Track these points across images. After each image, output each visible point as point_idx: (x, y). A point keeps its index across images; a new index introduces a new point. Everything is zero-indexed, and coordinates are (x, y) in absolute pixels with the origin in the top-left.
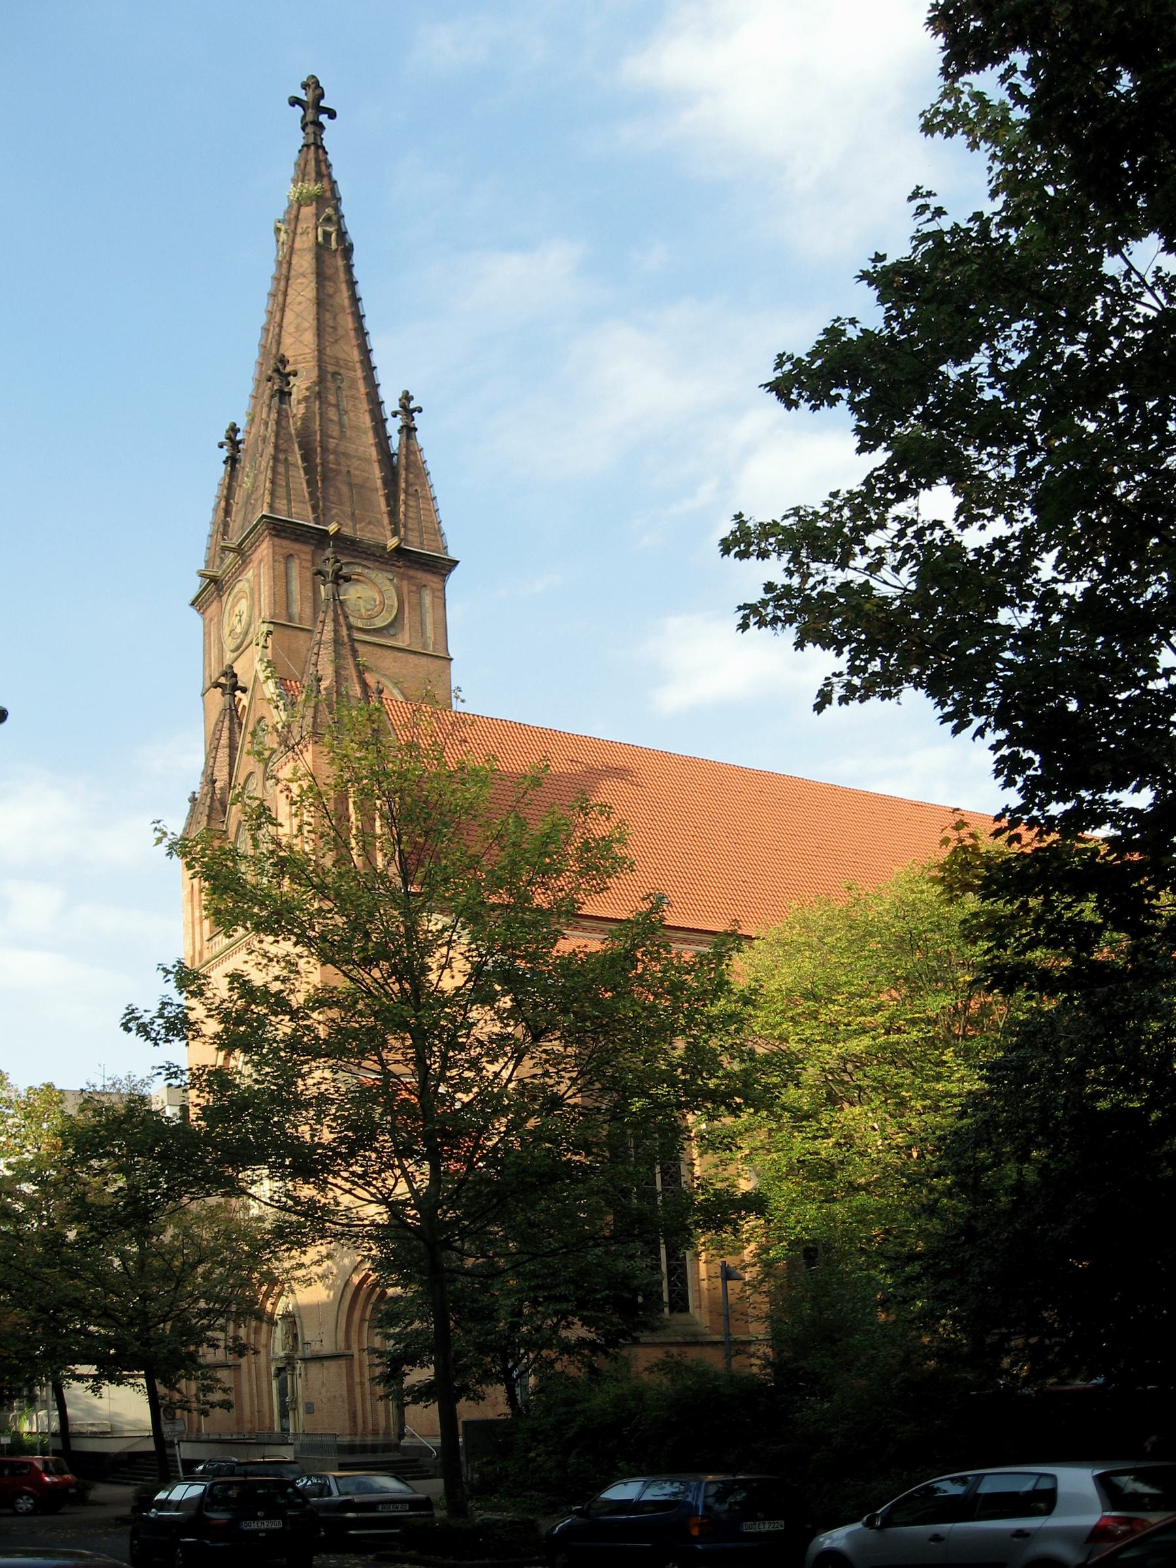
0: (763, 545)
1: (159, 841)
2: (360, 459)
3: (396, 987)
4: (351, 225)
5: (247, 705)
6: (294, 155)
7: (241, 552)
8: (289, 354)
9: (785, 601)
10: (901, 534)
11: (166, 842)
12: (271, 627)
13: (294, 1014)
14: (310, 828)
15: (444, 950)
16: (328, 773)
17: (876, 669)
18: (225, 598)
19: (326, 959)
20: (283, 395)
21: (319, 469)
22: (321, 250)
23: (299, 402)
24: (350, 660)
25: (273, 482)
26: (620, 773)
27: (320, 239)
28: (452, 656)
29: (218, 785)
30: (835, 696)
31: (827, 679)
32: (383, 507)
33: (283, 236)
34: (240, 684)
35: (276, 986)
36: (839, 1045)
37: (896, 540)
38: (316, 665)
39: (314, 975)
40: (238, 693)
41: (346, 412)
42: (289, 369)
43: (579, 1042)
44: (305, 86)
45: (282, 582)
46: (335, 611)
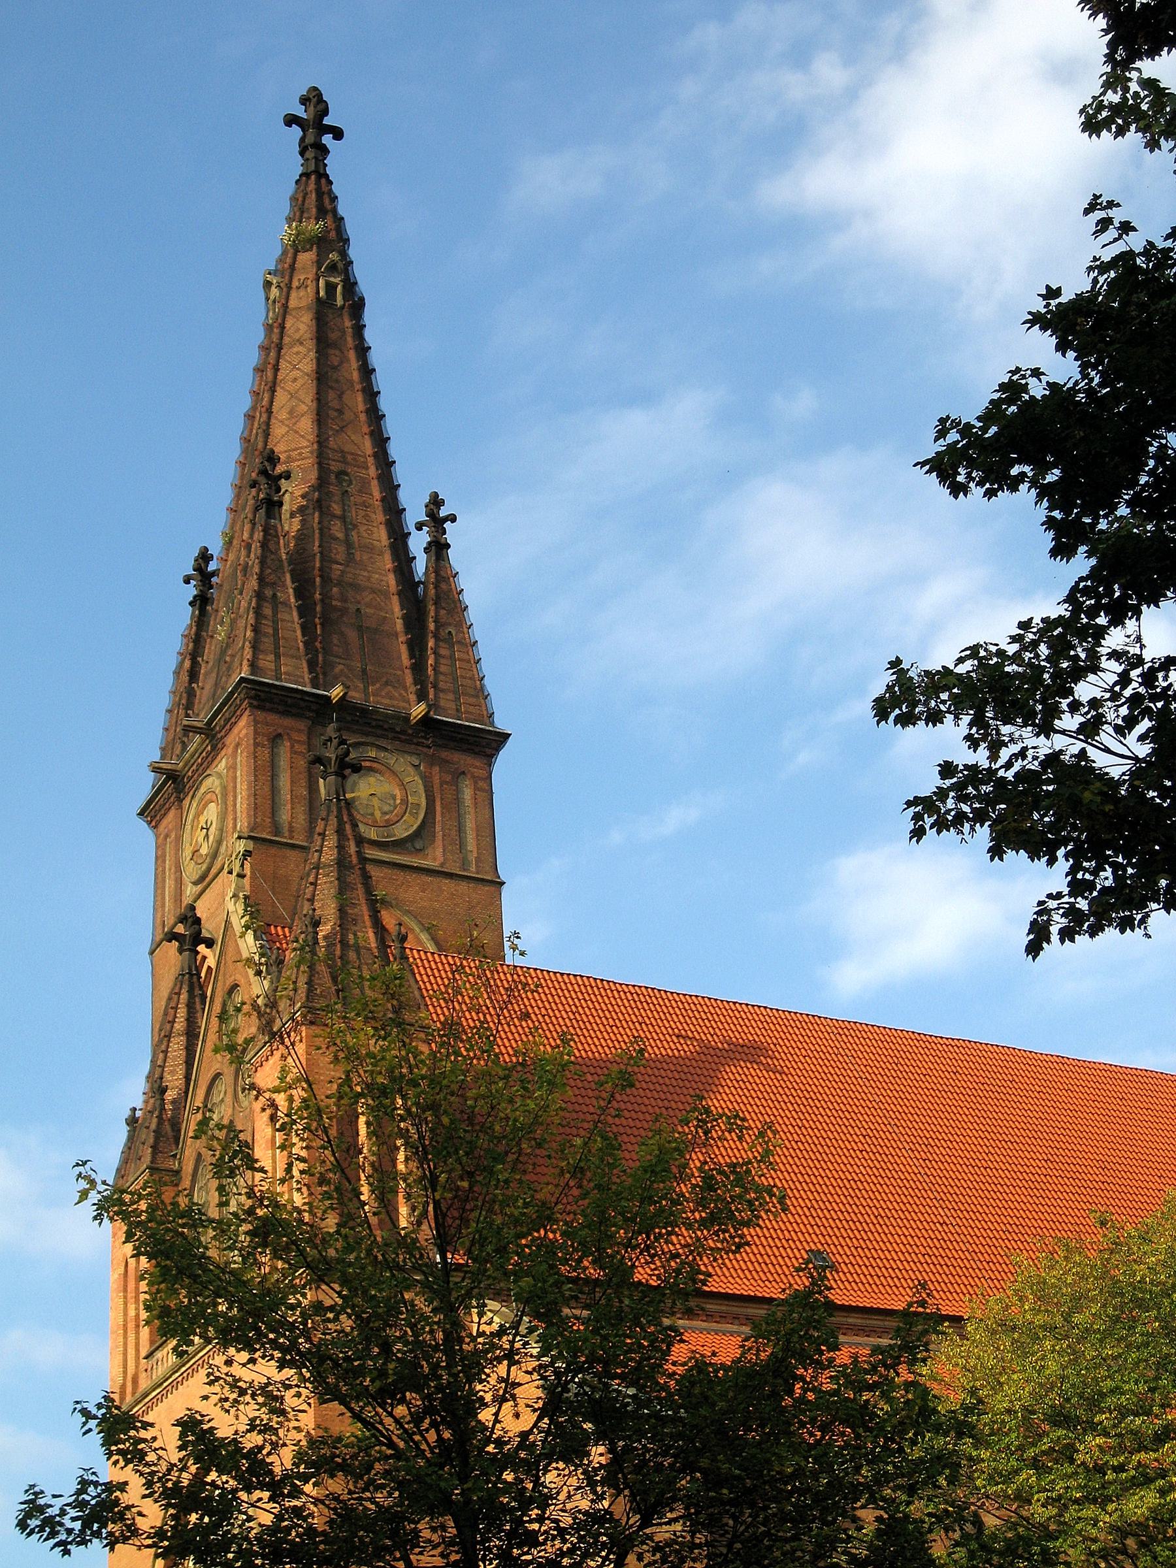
0: (933, 704)
1: (84, 1195)
2: (373, 591)
3: (432, 1436)
4: (361, 273)
5: (213, 966)
6: (290, 188)
7: (213, 735)
8: (280, 449)
9: (970, 789)
10: (1124, 679)
11: (94, 1197)
12: (251, 845)
13: (278, 1488)
14: (302, 1166)
15: (502, 1369)
16: (329, 1075)
17: (1107, 884)
18: (186, 802)
19: (325, 1393)
20: (272, 506)
21: (318, 608)
22: (323, 309)
23: (292, 515)
24: (361, 891)
25: (255, 630)
26: (751, 1052)
27: (322, 293)
28: (503, 878)
29: (170, 1095)
30: (1054, 930)
31: (1040, 903)
32: (406, 660)
33: (274, 292)
34: (205, 934)
35: (253, 1440)
36: (1111, 1507)
37: (1117, 688)
38: (311, 900)
39: (305, 1415)
40: (201, 948)
41: (355, 526)
42: (279, 469)
43: (712, 1524)
44: (304, 101)
45: (266, 774)
46: (339, 817)
